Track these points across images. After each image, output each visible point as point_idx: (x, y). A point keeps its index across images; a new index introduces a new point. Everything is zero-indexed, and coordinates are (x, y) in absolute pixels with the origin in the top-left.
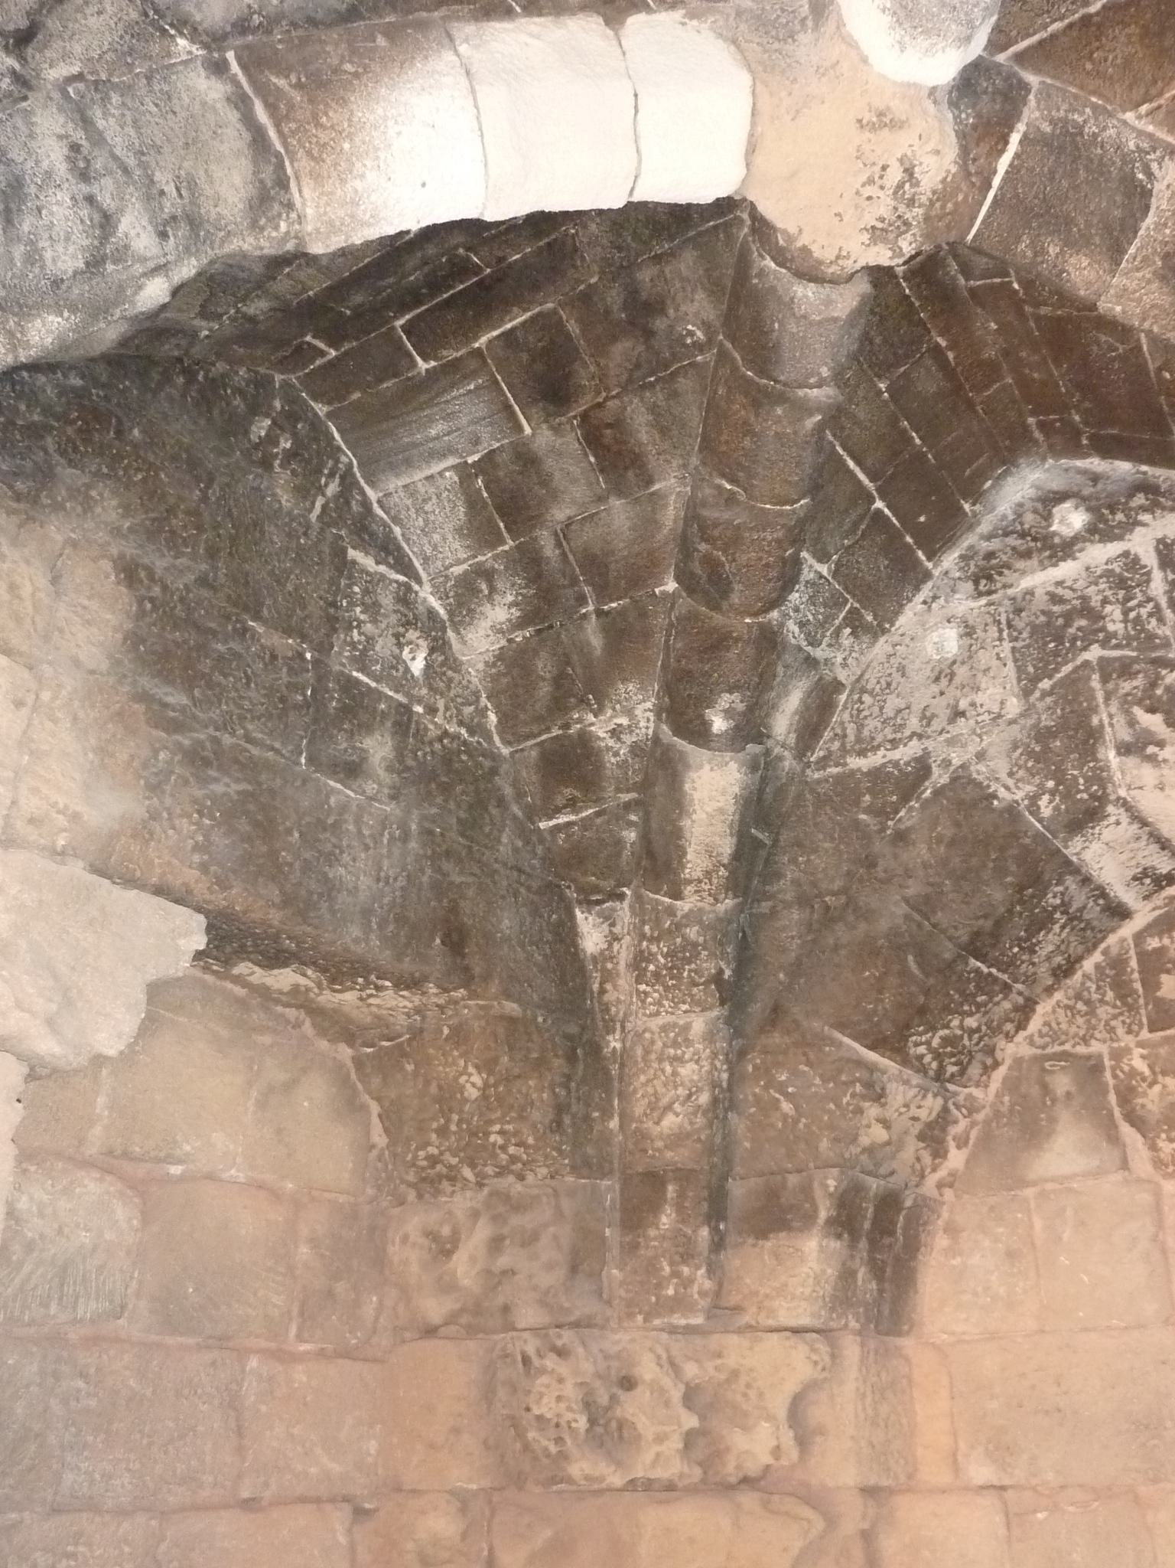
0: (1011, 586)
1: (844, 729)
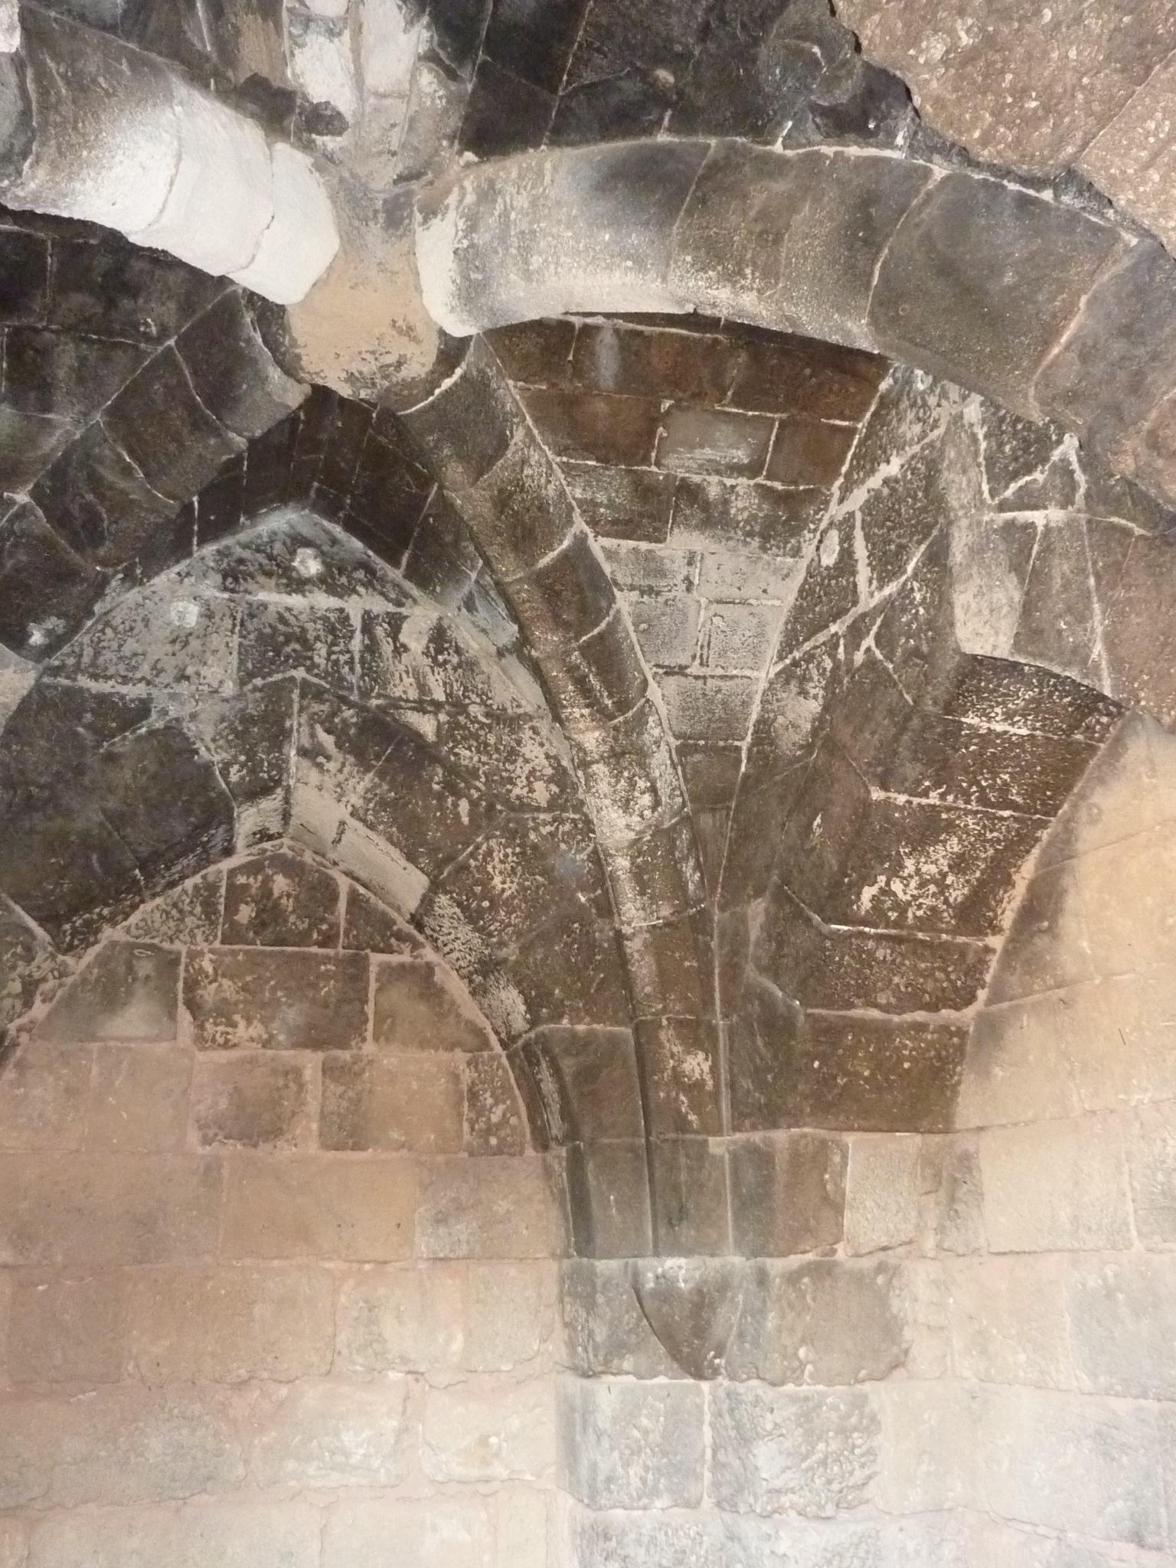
0: (250, 593)
1: (82, 650)
